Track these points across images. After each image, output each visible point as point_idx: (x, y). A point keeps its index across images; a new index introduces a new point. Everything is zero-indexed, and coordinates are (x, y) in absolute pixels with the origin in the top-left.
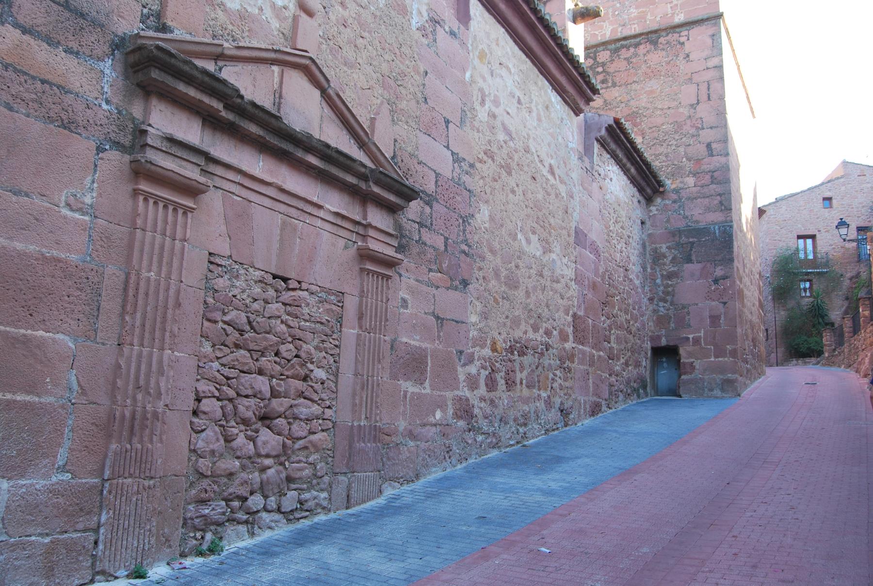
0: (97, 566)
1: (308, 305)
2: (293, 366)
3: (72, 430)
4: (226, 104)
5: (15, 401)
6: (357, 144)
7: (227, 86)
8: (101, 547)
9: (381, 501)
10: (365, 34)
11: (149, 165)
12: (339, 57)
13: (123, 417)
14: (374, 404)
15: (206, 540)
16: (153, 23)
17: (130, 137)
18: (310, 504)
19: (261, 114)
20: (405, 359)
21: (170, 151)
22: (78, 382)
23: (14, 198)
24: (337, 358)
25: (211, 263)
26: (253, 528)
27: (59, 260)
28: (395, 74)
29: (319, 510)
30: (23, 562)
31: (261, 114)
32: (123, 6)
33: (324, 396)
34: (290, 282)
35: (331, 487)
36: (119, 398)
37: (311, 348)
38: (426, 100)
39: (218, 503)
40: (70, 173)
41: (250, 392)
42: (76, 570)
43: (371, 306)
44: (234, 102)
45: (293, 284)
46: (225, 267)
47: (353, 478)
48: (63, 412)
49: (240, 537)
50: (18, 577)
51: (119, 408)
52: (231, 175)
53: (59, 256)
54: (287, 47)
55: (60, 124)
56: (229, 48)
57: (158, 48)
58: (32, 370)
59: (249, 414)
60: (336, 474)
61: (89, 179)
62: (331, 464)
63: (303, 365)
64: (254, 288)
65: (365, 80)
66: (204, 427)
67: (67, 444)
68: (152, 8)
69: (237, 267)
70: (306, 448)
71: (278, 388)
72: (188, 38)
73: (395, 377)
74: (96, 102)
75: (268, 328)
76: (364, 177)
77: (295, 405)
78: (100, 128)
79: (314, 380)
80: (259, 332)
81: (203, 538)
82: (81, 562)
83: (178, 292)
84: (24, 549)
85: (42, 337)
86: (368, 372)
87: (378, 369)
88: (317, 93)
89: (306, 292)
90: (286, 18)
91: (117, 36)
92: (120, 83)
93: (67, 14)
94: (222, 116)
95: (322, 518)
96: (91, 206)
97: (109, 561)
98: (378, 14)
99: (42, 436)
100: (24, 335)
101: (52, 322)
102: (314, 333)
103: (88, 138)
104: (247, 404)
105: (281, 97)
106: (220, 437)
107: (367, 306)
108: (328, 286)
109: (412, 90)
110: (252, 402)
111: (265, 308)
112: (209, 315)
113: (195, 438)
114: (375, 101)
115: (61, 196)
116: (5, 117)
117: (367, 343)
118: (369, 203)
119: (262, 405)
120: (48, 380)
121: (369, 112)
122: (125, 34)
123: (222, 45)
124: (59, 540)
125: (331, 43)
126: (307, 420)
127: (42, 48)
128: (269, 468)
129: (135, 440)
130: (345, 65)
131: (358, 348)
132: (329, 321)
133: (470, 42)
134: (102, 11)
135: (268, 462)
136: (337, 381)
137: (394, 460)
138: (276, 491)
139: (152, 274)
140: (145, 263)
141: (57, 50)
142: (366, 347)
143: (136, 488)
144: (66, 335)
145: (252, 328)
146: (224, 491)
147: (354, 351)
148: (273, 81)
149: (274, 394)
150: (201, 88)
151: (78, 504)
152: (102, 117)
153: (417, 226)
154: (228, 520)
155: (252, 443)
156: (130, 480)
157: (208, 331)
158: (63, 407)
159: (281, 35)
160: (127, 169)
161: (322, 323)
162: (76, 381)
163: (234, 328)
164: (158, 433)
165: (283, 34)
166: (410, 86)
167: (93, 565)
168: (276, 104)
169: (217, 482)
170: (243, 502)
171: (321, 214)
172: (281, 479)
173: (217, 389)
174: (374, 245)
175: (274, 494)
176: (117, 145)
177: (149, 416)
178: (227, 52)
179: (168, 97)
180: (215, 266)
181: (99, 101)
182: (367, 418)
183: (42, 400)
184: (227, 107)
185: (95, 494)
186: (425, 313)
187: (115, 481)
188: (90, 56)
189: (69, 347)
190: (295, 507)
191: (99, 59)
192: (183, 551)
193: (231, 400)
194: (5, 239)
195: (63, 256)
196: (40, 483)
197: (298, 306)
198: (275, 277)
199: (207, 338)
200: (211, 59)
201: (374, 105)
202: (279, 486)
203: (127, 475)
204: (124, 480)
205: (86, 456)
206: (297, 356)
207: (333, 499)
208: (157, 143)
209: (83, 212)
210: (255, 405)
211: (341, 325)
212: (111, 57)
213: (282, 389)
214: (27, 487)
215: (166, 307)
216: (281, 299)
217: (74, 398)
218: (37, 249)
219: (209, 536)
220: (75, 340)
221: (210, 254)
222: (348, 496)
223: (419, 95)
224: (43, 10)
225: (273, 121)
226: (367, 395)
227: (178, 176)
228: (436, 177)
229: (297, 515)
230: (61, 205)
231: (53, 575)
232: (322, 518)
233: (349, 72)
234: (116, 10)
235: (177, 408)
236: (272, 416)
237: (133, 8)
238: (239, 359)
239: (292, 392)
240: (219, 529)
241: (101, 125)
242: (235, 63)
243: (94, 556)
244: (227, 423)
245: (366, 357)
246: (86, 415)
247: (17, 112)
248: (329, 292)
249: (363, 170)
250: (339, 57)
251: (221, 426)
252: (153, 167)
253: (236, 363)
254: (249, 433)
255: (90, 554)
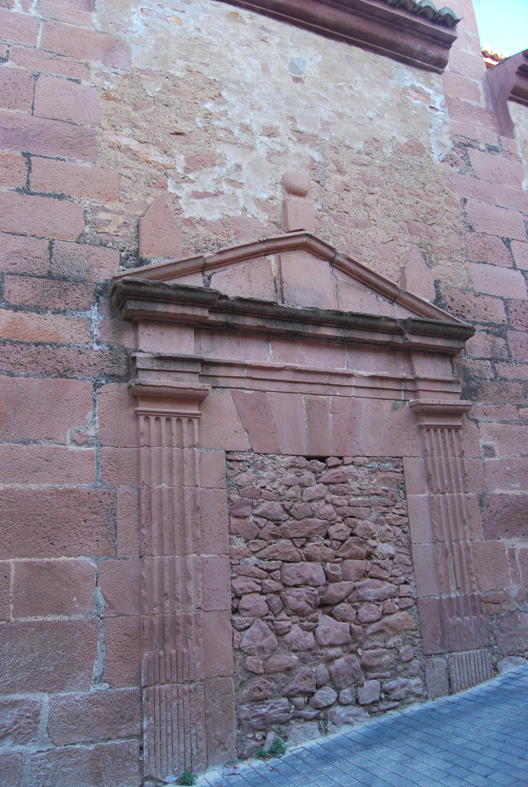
0: (145, 771)
1: (356, 479)
2: (349, 546)
3: (105, 643)
4: (212, 308)
5: (46, 622)
6: (387, 300)
7: (205, 292)
8: (145, 753)
9: (495, 682)
10: (376, 189)
11: (140, 388)
12: (347, 222)
13: (152, 624)
14: (466, 572)
15: (267, 741)
16: (133, 262)
17: (125, 367)
18: (397, 692)
19: (252, 306)
20: (503, 513)
21: (162, 369)
22: (105, 597)
23: (25, 448)
24: (407, 528)
25: (231, 461)
26: (326, 724)
27: (72, 491)
28: (422, 216)
29: (412, 699)
30: (71, 769)
31: (252, 306)
32: (101, 258)
33: (395, 572)
34: (329, 459)
35: (424, 671)
36: (146, 607)
37: (369, 523)
38: (471, 227)
39: (278, 701)
40: (72, 413)
41: (298, 581)
42: (124, 775)
43: (441, 464)
44: (219, 304)
45: (332, 461)
46: (246, 461)
47: (452, 659)
48: (93, 627)
49: (308, 735)
50: (67, 783)
51: (147, 617)
52: (236, 372)
53: (71, 488)
54: (281, 233)
55: (56, 374)
56: (210, 257)
57: (126, 282)
58: (59, 592)
59: (302, 604)
60: (429, 656)
61: (90, 414)
62: (420, 645)
63: (362, 542)
64: (286, 475)
65: (385, 233)
66: (247, 624)
67: (101, 656)
68: (130, 249)
69: (261, 458)
70: (381, 631)
71: (332, 572)
72: (168, 261)
73: (493, 536)
74: (87, 347)
75: (310, 513)
76: (397, 331)
77: (359, 587)
78: (94, 368)
79: (380, 557)
80: (298, 518)
81: (264, 738)
82: (128, 767)
83: (195, 497)
84: (71, 757)
85: (64, 562)
86: (450, 536)
87: (464, 531)
88: (325, 265)
89: (352, 466)
90: (274, 208)
91: (99, 285)
92: (108, 323)
93: (51, 283)
94: (211, 321)
95: (416, 707)
96: (96, 437)
97: (156, 767)
98: (386, 164)
99: (76, 651)
100: (48, 563)
101: (72, 547)
102: (370, 507)
103: (84, 379)
104: (297, 594)
105: (282, 282)
106: (269, 632)
107: (434, 465)
108: (379, 453)
109: (449, 223)
110: (303, 590)
111: (302, 492)
112: (236, 512)
113: (238, 637)
114: (402, 250)
115: (66, 435)
116: (8, 383)
117: (442, 505)
118: (413, 356)
119: (316, 592)
120: (75, 600)
121: (398, 263)
122: (106, 280)
123: (202, 257)
124: (102, 747)
125: (334, 212)
126: (379, 601)
127: (32, 317)
128: (337, 658)
129: (168, 646)
130: (357, 227)
131: (432, 512)
132: (387, 491)
133: (520, 149)
134: (82, 269)
135: (332, 652)
136: (411, 553)
137: (511, 630)
138: (350, 682)
139: (164, 485)
140: (154, 477)
141: (46, 315)
142: (442, 510)
143: (175, 693)
144: (87, 556)
145: (291, 515)
146: (283, 687)
147: (428, 517)
148: (271, 270)
149: (330, 578)
150: (180, 303)
151: (118, 712)
152: (95, 357)
153: (489, 363)
154: (294, 718)
155: (311, 634)
156: (168, 685)
157: (237, 527)
158: (92, 622)
159: (273, 225)
160: (125, 395)
161: (378, 495)
162: (102, 597)
163: (268, 520)
164: (193, 637)
165: (274, 223)
166: (446, 220)
167: (141, 770)
168: (279, 290)
169: (273, 679)
170: (309, 697)
171: (354, 382)
172: (354, 669)
173: (258, 584)
174: (426, 399)
175: (349, 686)
176: (113, 377)
177: (180, 621)
178: (208, 261)
179: (154, 321)
180: (235, 463)
181: (90, 344)
182: (458, 588)
183: (72, 618)
184: (213, 310)
185: (134, 702)
186: (523, 456)
187: (151, 688)
188: (77, 309)
189: (91, 566)
190: (377, 698)
191: (85, 309)
192: (242, 753)
193: (277, 592)
194: (21, 483)
195: (75, 487)
196: (79, 694)
197: (344, 483)
198: (309, 458)
199: (237, 534)
200: (197, 272)
201: (402, 254)
202: (353, 676)
203: (163, 680)
204: (162, 686)
205: (122, 666)
206: (352, 535)
207: (429, 684)
208: (148, 365)
209: (89, 444)
210: (307, 593)
211: (405, 492)
212: (97, 304)
213: (338, 573)
214: (67, 699)
215: (183, 514)
216: (321, 479)
217: (102, 613)
218: (50, 486)
219: (271, 736)
220: (96, 560)
221: (227, 452)
222: (449, 680)
223: (461, 226)
224: (30, 287)
225: (267, 308)
226: (454, 562)
227: (171, 389)
228: (505, 304)
229: (383, 706)
230: (67, 443)
231: (101, 781)
232: (416, 707)
233: (363, 232)
234: (95, 264)
235: (213, 609)
236: (331, 602)
237: (111, 256)
238: (279, 549)
239: (353, 573)
240: (283, 728)
241: (95, 364)
242: (225, 268)
243: (141, 762)
244: (275, 616)
245: (444, 520)
246: (116, 627)
247: (18, 376)
248: (381, 460)
249: (392, 324)
250: (347, 222)
251: (268, 620)
252: (144, 388)
253: (276, 554)
254: (306, 623)
255: (136, 759)
